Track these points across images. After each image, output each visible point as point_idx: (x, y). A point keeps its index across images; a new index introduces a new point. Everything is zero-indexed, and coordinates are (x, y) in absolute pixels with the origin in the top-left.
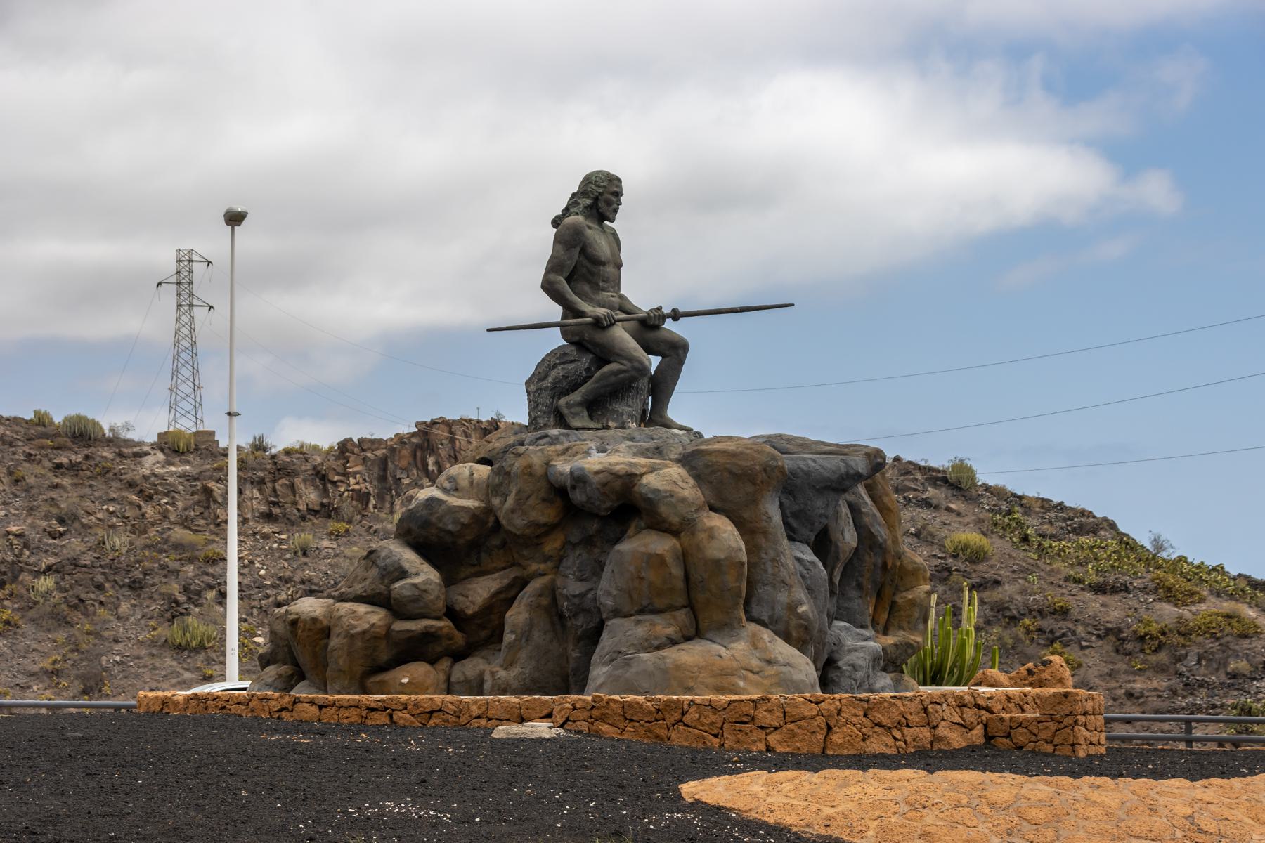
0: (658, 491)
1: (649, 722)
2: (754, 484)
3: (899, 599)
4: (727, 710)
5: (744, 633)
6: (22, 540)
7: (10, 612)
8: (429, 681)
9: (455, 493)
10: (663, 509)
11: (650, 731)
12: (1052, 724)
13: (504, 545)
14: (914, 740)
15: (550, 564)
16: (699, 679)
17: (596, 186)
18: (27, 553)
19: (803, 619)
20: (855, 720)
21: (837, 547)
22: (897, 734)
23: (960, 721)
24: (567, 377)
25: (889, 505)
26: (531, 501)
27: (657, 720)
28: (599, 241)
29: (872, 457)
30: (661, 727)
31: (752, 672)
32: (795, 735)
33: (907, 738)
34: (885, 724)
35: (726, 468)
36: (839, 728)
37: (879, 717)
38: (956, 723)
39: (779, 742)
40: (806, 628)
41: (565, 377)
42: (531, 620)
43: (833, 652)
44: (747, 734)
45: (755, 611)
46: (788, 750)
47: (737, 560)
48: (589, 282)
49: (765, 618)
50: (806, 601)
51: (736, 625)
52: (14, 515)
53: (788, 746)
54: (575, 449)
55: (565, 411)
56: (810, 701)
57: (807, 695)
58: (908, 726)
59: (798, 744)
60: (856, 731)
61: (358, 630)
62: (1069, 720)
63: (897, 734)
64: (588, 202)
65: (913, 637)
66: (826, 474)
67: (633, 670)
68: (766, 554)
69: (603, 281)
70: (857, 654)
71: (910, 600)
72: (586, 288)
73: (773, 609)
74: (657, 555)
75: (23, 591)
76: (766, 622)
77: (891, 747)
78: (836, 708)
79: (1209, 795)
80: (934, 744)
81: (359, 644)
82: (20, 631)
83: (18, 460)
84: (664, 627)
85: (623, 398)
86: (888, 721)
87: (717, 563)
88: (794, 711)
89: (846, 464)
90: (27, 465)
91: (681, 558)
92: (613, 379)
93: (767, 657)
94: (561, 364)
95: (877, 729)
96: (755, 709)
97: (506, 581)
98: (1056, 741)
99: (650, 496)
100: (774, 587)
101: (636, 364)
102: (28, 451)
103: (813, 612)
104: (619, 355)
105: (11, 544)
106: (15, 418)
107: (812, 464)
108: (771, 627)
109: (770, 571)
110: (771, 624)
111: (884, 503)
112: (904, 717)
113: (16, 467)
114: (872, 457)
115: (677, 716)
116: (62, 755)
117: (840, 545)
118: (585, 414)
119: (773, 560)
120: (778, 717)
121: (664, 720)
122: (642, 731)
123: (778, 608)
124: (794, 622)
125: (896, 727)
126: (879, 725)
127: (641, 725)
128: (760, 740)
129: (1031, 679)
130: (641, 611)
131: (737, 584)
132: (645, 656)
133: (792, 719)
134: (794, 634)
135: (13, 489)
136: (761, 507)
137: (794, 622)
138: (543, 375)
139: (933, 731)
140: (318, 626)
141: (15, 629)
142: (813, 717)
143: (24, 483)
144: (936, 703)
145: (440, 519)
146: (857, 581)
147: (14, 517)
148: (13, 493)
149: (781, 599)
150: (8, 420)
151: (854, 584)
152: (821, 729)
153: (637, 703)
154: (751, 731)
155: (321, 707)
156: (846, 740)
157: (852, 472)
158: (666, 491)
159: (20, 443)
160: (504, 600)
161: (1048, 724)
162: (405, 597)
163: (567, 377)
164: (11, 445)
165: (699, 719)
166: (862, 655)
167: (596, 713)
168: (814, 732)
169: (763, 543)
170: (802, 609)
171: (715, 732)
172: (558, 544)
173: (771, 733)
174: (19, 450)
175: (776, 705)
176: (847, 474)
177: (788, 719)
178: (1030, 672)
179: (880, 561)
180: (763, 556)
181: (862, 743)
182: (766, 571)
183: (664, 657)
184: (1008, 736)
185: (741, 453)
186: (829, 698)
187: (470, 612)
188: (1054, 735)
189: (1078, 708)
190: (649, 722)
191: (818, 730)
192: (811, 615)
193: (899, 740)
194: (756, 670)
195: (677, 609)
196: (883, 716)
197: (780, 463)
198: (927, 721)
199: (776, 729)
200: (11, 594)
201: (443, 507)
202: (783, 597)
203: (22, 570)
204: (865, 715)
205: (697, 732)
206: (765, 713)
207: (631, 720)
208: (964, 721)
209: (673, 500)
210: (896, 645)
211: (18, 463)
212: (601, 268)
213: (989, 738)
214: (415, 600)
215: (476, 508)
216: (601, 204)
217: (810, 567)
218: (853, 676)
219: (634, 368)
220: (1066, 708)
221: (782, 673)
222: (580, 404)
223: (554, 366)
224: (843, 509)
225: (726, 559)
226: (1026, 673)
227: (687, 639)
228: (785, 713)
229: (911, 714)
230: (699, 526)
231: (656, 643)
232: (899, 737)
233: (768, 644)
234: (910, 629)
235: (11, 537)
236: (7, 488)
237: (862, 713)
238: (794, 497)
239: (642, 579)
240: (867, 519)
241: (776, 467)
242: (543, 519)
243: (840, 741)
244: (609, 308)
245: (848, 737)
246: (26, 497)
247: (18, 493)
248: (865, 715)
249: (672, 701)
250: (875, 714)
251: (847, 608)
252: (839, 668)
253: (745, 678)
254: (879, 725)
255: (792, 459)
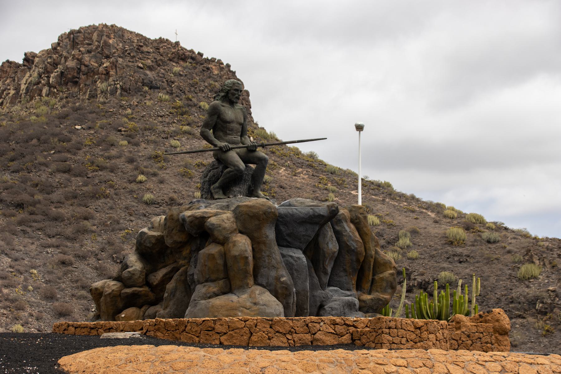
0: (214, 224)
1: (173, 331)
2: (259, 220)
3: (376, 277)
4: (202, 325)
5: (249, 291)
6: (555, 293)
7: (549, 326)
8: (134, 316)
9: (153, 230)
10: (216, 233)
11: (173, 335)
12: (374, 333)
13: (171, 253)
14: (300, 340)
15: (186, 261)
16: (220, 312)
17: (227, 87)
18: (558, 299)
19: (285, 284)
20: (265, 330)
21: (323, 251)
22: (289, 337)
23: (333, 331)
24: (214, 176)
25: (366, 231)
26: (174, 232)
27: (176, 330)
28: (227, 112)
29: (330, 207)
30: (177, 334)
31: (246, 308)
32: (233, 337)
33: (295, 339)
34: (281, 331)
35: (246, 213)
36: (256, 333)
37: (278, 328)
38: (329, 333)
39: (226, 340)
40: (286, 288)
41: (214, 176)
42: (176, 286)
43: (323, 301)
44: (210, 336)
45: (260, 280)
46: (230, 344)
47: (244, 256)
48: (222, 131)
49: (264, 284)
50: (285, 275)
51: (246, 287)
52: (552, 282)
53: (230, 342)
54: (193, 207)
55: (213, 191)
56: (241, 320)
57: (240, 318)
58: (296, 333)
59: (235, 341)
60: (265, 335)
61: (107, 293)
62: (380, 331)
63: (289, 337)
64: (223, 94)
65: (382, 296)
66: (302, 215)
67: (197, 308)
68: (265, 253)
69: (229, 130)
70: (335, 302)
71: (381, 278)
72: (221, 134)
73: (268, 279)
74: (212, 254)
75: (556, 317)
76: (265, 285)
77: (285, 343)
78: (254, 324)
79: (284, 358)
80: (314, 342)
81: (109, 299)
82: (554, 335)
83: (554, 257)
84: (213, 288)
85: (238, 184)
86: (284, 330)
87: (235, 257)
88: (233, 325)
89: (313, 210)
90: (558, 259)
91: (224, 256)
92: (228, 175)
93: (254, 301)
94: (212, 169)
95: (277, 334)
96: (215, 324)
97: (170, 269)
98: (376, 342)
99: (210, 227)
100: (269, 269)
101: (236, 168)
102: (559, 253)
103: (290, 281)
104: (230, 164)
105: (550, 295)
106: (554, 239)
107: (295, 211)
108: (267, 288)
109: (267, 261)
110: (267, 286)
111: (364, 231)
112: (292, 328)
113: (553, 260)
114: (330, 207)
115: (183, 328)
116: (135, 363)
117: (325, 250)
118: (221, 192)
119: (268, 256)
120: (225, 328)
121: (179, 330)
122: (171, 335)
123: (271, 279)
124: (279, 285)
125: (289, 333)
126: (278, 332)
127: (171, 333)
128: (217, 339)
129: (481, 320)
130: (207, 281)
131: (244, 267)
132: (203, 301)
133: (232, 329)
134: (280, 291)
135: (552, 270)
136: (263, 231)
137: (279, 285)
138: (206, 175)
139: (312, 336)
140: (98, 292)
141: (551, 334)
142: (242, 328)
143: (557, 268)
144: (314, 322)
145: (144, 241)
146: (343, 268)
147: (552, 283)
148: (551, 272)
149: (272, 274)
150: (551, 239)
151: (342, 269)
152: (247, 334)
153: (169, 322)
154: (212, 335)
155: (76, 328)
156: (259, 339)
157: (316, 214)
158: (217, 225)
159: (556, 250)
160: (167, 278)
161: (373, 333)
162: (126, 277)
163: (214, 176)
164: (551, 250)
165: (191, 329)
166: (338, 303)
167: (156, 327)
168: (242, 335)
169: (263, 247)
170: (283, 279)
171: (198, 335)
172: (188, 251)
173: (222, 335)
174: (555, 253)
175: (225, 322)
176: (314, 215)
177: (230, 329)
178: (480, 316)
179: (354, 258)
180: (264, 254)
181: (268, 341)
182: (265, 261)
183: (210, 302)
184: (360, 340)
185: (254, 206)
186: (251, 319)
187: (155, 284)
188: (375, 339)
189: (384, 325)
190: (173, 331)
191: (245, 334)
192: (289, 282)
193: (291, 340)
194: (248, 307)
195: (221, 279)
196: (280, 328)
197: (273, 210)
198: (308, 330)
199: (225, 334)
200: (550, 318)
201: (146, 236)
202: (273, 273)
203: (555, 307)
204: (271, 327)
205: (190, 335)
206: (219, 326)
207: (168, 330)
208: (336, 332)
209: (220, 228)
210: (372, 299)
211: (554, 258)
212: (228, 124)
213: (353, 340)
214: (130, 278)
215: (158, 236)
216: (230, 95)
217: (297, 260)
218: (331, 313)
219: (237, 171)
220: (378, 326)
221: (260, 309)
222: (218, 188)
223: (210, 171)
224: (329, 233)
225: (239, 255)
226: (478, 317)
227: (224, 293)
228: (229, 326)
229: (298, 327)
230: (230, 240)
231: (209, 295)
232: (290, 338)
233: (257, 295)
234: (382, 292)
235: (550, 292)
236: (549, 270)
237: (268, 326)
238: (287, 226)
239: (206, 265)
240: (345, 238)
241: (271, 212)
242: (179, 240)
243: (256, 340)
244: (227, 142)
245: (260, 338)
246: (557, 274)
247: (554, 272)
248: (271, 327)
249: (181, 321)
250: (276, 327)
251: (338, 281)
252: (325, 309)
253: (242, 311)
254: (278, 332)
255: (286, 209)
